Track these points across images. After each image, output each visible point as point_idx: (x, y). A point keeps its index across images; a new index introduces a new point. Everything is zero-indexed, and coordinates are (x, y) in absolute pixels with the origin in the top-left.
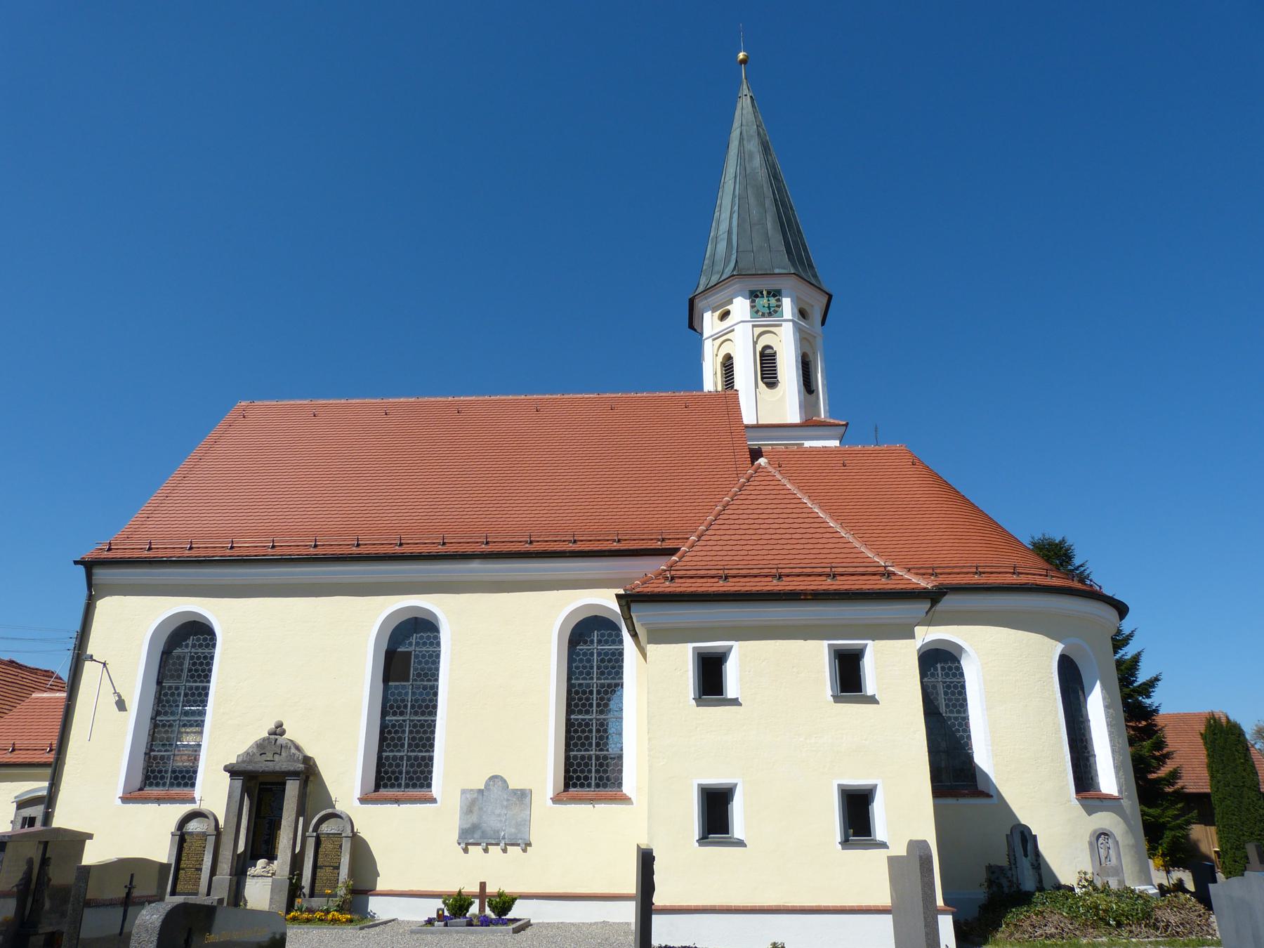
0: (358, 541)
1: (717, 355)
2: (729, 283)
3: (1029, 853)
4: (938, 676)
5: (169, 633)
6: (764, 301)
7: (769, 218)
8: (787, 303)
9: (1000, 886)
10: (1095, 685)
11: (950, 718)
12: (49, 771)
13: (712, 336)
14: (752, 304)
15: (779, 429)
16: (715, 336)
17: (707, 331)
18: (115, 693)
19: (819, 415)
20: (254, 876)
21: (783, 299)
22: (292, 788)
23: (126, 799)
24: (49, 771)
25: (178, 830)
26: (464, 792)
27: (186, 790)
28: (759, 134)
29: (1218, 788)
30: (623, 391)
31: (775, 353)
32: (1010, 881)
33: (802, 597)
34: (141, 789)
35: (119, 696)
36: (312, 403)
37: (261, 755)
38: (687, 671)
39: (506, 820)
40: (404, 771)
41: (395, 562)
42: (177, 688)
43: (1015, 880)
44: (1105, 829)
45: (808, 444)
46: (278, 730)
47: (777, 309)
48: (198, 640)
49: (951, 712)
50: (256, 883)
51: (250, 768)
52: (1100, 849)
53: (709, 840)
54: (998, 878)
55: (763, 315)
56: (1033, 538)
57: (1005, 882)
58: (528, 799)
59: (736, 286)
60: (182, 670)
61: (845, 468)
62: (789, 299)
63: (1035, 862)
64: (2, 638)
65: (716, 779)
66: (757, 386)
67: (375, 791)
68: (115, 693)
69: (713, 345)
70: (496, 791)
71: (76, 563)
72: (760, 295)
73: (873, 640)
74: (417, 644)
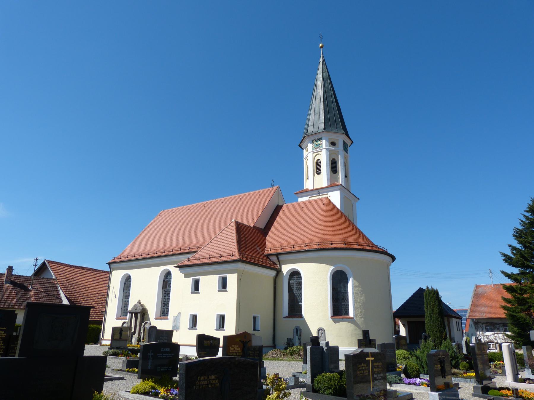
8: (324, 142)
11: (296, 293)
22: (139, 316)
26: (173, 317)
27: (166, 317)
30: (265, 188)
34: (121, 317)
46: (139, 302)
51: (131, 311)
55: (316, 148)
56: (531, 198)
62: (325, 140)
63: (299, 338)
65: (221, 313)
71: (107, 263)
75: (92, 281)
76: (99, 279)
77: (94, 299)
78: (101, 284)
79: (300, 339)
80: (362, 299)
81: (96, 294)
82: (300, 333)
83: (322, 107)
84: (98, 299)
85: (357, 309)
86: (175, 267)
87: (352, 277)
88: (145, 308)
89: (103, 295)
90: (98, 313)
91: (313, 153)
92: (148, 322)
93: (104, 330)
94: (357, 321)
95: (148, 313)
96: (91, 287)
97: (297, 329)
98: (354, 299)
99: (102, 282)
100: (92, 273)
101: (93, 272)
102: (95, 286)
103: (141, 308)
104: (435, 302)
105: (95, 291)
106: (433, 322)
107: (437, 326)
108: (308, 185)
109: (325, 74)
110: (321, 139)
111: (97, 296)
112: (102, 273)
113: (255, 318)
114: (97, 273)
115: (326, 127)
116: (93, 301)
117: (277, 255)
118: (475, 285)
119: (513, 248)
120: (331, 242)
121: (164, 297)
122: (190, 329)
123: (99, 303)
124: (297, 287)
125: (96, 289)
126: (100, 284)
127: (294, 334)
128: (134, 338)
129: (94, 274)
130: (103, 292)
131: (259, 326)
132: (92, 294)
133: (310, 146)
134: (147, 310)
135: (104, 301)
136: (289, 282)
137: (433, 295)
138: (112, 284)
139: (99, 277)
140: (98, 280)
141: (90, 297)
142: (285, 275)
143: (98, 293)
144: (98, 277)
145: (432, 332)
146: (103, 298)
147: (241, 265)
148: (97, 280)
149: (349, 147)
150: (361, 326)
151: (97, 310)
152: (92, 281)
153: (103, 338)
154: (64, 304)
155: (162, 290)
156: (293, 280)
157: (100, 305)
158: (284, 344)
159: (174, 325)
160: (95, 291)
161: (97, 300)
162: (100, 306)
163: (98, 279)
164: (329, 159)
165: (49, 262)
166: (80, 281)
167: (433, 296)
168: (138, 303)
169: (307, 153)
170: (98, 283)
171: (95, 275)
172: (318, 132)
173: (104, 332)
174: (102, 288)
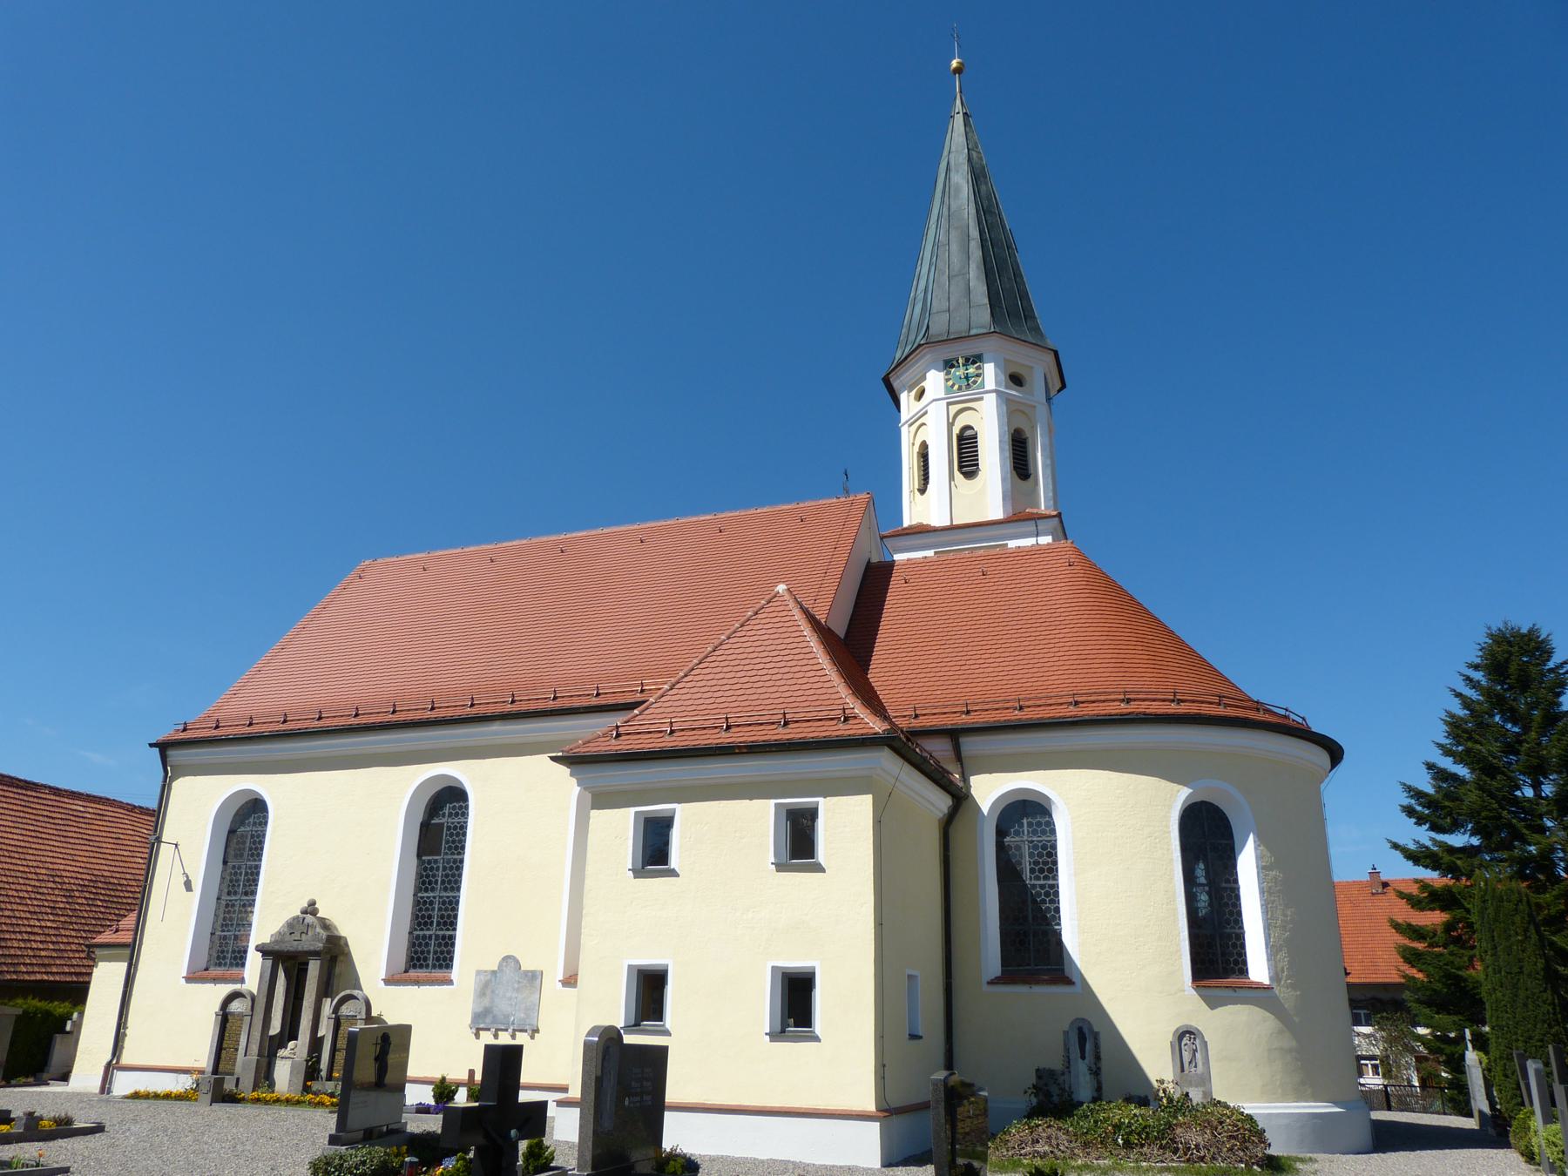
0: (642, 686)
1: (913, 444)
2: (922, 353)
3: (1087, 1055)
4: (1024, 834)
5: (427, 800)
6: (960, 372)
7: (973, 266)
8: (989, 369)
9: (1048, 1095)
10: (1247, 840)
11: (1034, 886)
12: (127, 952)
13: (907, 422)
14: (946, 377)
15: (989, 527)
16: (912, 421)
17: (905, 415)
18: (184, 873)
19: (1037, 505)
20: (282, 1058)
21: (985, 365)
22: (314, 968)
23: (189, 979)
24: (127, 952)
25: (333, 1013)
26: (478, 973)
27: (235, 971)
28: (970, 159)
29: (1487, 976)
32: (1061, 1089)
33: (737, 751)
34: (206, 969)
35: (187, 876)
36: (717, 517)
37: (291, 934)
39: (516, 1004)
40: (432, 951)
41: (531, 720)
42: (240, 868)
43: (1067, 1089)
44: (1191, 1026)
45: (1012, 544)
46: (311, 909)
47: (976, 379)
48: (454, 808)
49: (1038, 878)
50: (284, 1065)
51: (277, 948)
52: (1183, 1051)
53: (641, 1027)
54: (1046, 1085)
55: (960, 389)
56: (1489, 628)
57: (1055, 1090)
58: (538, 981)
59: (928, 356)
60: (244, 849)
61: (1072, 568)
62: (992, 365)
65: (649, 959)
66: (951, 477)
67: (405, 972)
68: (184, 873)
69: (909, 432)
70: (508, 972)
71: (151, 745)
72: (956, 364)
73: (825, 797)
74: (450, 815)
75: (10, 824)
76: (37, 818)
77: (21, 895)
78: (47, 836)
79: (1096, 1072)
80: (1289, 913)
81: (30, 876)
82: (1097, 1046)
84: (38, 896)
86: (552, 758)
87: (1254, 834)
88: (336, 933)
89: (57, 879)
90: (43, 950)
92: (355, 992)
93: (125, 1028)
94: (1280, 998)
96: (10, 848)
97: (1080, 1030)
99: (51, 831)
100: (11, 795)
101: (15, 790)
102: (23, 844)
103: (324, 934)
104: (1526, 930)
105: (24, 863)
106: (1525, 1005)
107: (1544, 1022)
109: (974, 154)
110: (976, 359)
111: (33, 883)
112: (48, 797)
114: (29, 793)
116: (18, 901)
117: (954, 735)
119: (1440, 775)
120: (1125, 693)
121: (229, 893)
123: (43, 910)
124: (1036, 863)
125: (28, 857)
126: (43, 836)
127: (1067, 1050)
128: (289, 1062)
129: (17, 796)
130: (56, 867)
132: (13, 874)
133: (935, 381)
134: (347, 944)
135: (62, 905)
137: (1517, 905)
139: (39, 812)
140: (34, 823)
141: (7, 886)
142: (986, 814)
143: (38, 871)
144: (34, 812)
145: (1526, 1042)
146: (57, 892)
148: (30, 822)
151: (38, 938)
152: (10, 824)
153: (114, 1062)
156: (1017, 833)
157: (46, 918)
158: (1026, 1092)
159: (479, 1010)
160: (24, 863)
161: (35, 899)
162: (49, 924)
163: (33, 817)
164: (1006, 429)
167: (1516, 910)
168: (305, 912)
169: (917, 407)
170: (33, 834)
171: (23, 803)
173: (125, 1035)
174: (51, 854)
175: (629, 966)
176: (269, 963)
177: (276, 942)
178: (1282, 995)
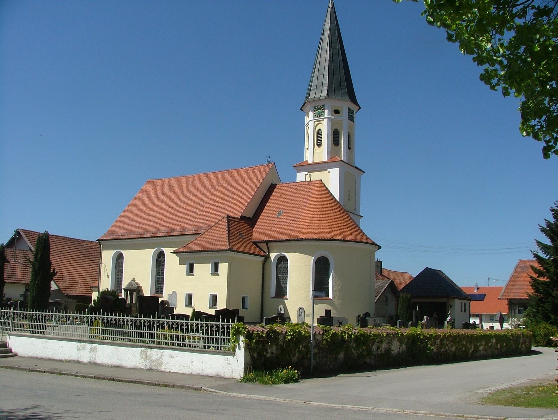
8: (326, 111)
19: (340, 157)
22: (135, 293)
24: (97, 288)
31: (322, 132)
38: (290, 274)
46: (134, 280)
51: (127, 289)
62: (327, 110)
64: (2, 367)
83: (327, 68)
85: (335, 292)
88: (139, 286)
91: (314, 122)
95: (142, 290)
98: (334, 283)
103: (136, 286)
108: (308, 157)
113: (244, 298)
115: (329, 92)
117: (267, 242)
118: (519, 260)
121: (158, 276)
122: (186, 306)
131: (248, 305)
133: (311, 114)
136: (277, 266)
138: (103, 261)
147: (231, 254)
149: (356, 113)
150: (338, 307)
154: (145, 295)
155: (155, 269)
165: (25, 231)
166: (88, 264)
172: (320, 99)
175: (186, 294)
176: (126, 292)
177: (127, 288)
178: (335, 301)
